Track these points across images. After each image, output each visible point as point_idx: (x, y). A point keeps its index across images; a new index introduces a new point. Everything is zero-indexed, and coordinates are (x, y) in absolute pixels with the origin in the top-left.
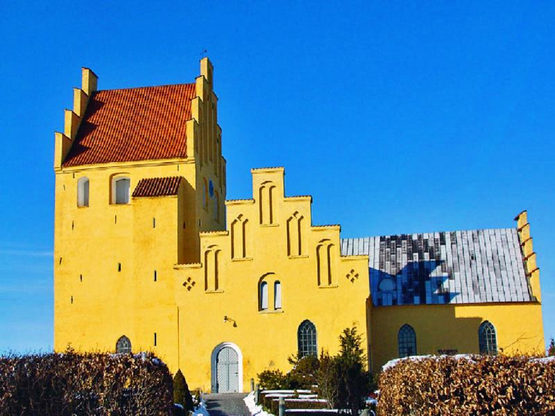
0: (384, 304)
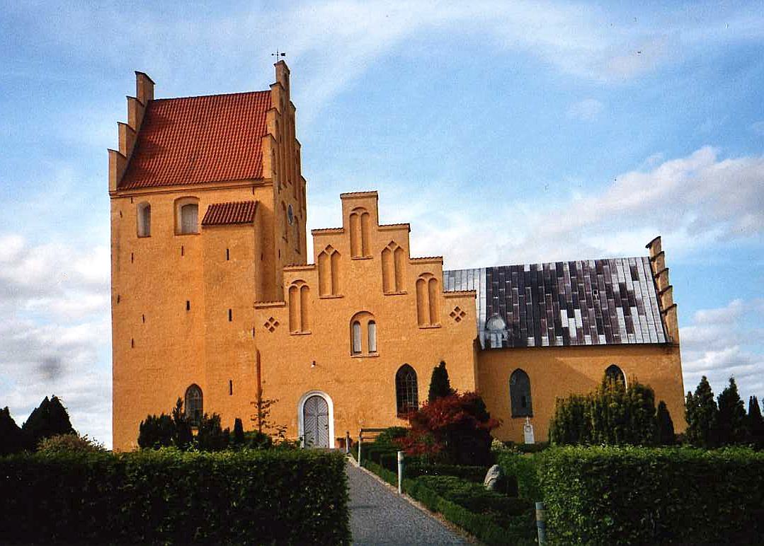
0: (493, 346)
